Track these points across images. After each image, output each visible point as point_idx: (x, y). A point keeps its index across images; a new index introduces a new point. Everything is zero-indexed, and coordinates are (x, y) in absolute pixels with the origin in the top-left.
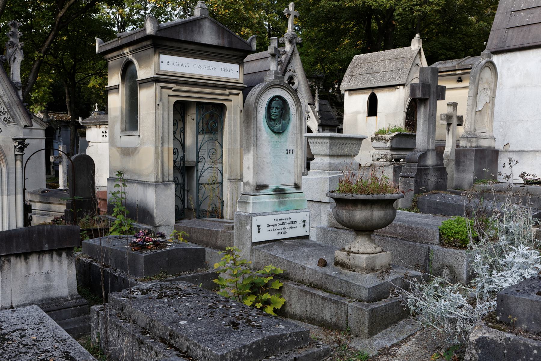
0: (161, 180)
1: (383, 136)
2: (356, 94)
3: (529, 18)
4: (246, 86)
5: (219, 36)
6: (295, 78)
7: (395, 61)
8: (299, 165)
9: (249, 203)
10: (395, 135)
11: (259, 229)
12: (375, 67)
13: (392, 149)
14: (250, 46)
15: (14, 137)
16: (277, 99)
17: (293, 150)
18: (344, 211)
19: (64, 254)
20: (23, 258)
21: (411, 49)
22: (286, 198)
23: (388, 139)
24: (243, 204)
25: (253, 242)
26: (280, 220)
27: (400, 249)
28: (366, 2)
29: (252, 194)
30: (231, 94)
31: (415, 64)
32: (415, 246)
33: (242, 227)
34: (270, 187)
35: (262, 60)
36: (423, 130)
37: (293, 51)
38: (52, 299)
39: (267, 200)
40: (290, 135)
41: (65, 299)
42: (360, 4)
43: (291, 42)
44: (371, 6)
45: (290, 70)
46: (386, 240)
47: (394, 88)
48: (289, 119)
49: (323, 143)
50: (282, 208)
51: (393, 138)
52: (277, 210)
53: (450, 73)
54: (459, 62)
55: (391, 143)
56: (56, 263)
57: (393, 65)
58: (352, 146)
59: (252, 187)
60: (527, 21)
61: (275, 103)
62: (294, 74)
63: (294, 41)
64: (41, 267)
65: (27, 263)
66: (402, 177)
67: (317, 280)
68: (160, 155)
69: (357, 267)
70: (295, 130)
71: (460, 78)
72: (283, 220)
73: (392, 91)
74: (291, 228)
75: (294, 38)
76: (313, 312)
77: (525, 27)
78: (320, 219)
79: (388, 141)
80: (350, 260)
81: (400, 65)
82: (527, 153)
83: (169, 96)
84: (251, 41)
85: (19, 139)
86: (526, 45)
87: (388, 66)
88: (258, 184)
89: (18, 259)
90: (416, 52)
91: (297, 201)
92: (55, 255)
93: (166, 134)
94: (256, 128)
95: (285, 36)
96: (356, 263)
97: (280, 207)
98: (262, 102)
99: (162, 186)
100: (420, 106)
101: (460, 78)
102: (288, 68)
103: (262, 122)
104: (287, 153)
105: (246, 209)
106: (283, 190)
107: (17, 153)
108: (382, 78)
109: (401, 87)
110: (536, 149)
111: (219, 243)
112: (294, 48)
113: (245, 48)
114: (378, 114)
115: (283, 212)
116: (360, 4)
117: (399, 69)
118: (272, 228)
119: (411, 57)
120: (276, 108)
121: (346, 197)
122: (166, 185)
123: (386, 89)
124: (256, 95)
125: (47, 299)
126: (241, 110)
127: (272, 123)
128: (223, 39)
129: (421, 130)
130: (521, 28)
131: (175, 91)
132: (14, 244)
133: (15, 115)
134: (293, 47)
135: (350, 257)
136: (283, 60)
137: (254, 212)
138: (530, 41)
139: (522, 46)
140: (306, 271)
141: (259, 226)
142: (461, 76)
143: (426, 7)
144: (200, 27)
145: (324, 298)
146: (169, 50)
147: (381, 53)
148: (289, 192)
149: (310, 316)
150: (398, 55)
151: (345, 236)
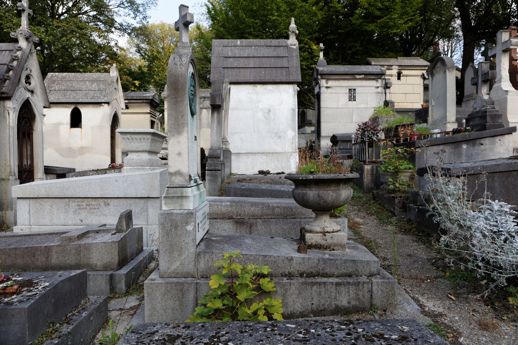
2: (57, 107)
3: (237, 63)
9: (186, 197)
12: (76, 85)
18: (330, 192)
21: (110, 75)
24: (175, 199)
27: (285, 227)
32: (301, 222)
33: (176, 228)
43: (27, 39)
45: (27, 68)
46: (269, 221)
47: (98, 106)
49: (142, 139)
57: (95, 86)
60: (235, 65)
62: (31, 73)
63: (31, 39)
66: (208, 170)
67: (312, 267)
69: (335, 245)
73: (97, 107)
76: (323, 302)
77: (236, 69)
78: (147, 215)
80: (326, 241)
81: (102, 86)
82: (242, 155)
86: (240, 81)
87: (90, 86)
96: (335, 242)
105: (181, 205)
108: (86, 95)
109: (106, 105)
110: (248, 152)
112: (32, 46)
114: (82, 126)
121: (339, 177)
123: (91, 106)
129: (215, 132)
130: (233, 69)
135: (327, 237)
138: (242, 79)
139: (237, 81)
140: (294, 261)
142: (127, 104)
145: (338, 284)
149: (318, 309)
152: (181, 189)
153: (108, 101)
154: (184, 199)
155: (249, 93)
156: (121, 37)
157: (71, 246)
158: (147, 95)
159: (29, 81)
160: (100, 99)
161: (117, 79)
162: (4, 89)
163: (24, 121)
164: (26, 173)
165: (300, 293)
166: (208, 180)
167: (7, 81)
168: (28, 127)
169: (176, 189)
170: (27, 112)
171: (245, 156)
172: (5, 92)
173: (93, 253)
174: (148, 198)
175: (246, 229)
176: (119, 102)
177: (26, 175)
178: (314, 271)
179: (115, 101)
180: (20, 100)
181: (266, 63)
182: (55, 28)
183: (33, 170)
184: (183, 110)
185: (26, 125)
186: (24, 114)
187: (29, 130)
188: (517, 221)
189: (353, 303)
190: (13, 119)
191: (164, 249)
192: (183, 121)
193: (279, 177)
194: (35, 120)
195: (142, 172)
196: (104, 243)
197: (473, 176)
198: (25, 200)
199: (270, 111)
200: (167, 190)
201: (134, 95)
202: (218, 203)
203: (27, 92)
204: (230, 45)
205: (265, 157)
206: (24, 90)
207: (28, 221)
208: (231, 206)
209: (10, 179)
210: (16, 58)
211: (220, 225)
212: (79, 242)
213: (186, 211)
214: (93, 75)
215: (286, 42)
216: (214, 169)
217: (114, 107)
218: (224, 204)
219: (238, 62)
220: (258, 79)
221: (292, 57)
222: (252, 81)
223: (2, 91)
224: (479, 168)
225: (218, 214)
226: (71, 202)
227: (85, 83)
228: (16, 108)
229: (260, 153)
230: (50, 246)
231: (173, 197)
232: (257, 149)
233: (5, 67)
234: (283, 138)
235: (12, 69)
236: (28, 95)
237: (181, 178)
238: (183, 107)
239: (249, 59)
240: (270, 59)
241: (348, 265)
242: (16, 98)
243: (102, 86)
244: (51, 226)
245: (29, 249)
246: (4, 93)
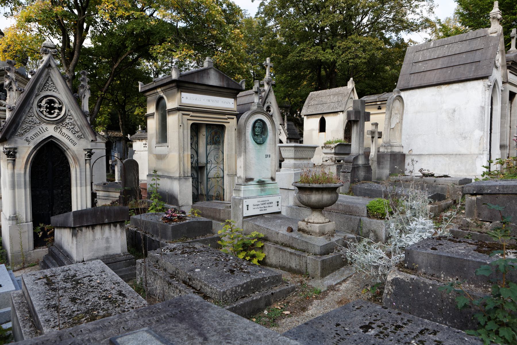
0: (182, 176)
1: (330, 145)
3: (425, 67)
5: (220, 80)
6: (271, 107)
9: (241, 190)
12: (324, 100)
13: (335, 154)
14: (241, 86)
15: (84, 148)
16: (259, 121)
19: (118, 226)
20: (90, 228)
27: (341, 220)
30: (229, 118)
32: (351, 218)
33: (236, 206)
34: (255, 180)
36: (356, 142)
38: (111, 256)
41: (119, 255)
43: (268, 84)
44: (321, 60)
47: (336, 114)
50: (263, 193)
51: (336, 147)
53: (373, 103)
55: (335, 150)
56: (113, 231)
57: (335, 99)
60: (423, 69)
63: (270, 83)
64: (103, 234)
65: (93, 231)
66: (342, 172)
68: (182, 159)
69: (313, 232)
74: (269, 206)
77: (422, 73)
78: (288, 201)
79: (333, 148)
81: (340, 98)
83: (188, 120)
84: (242, 83)
85: (88, 149)
88: (247, 178)
89: (88, 229)
90: (351, 90)
91: (273, 189)
92: (112, 226)
93: (186, 145)
94: (245, 140)
95: (264, 80)
96: (312, 229)
97: (261, 193)
99: (183, 180)
100: (353, 125)
101: (379, 107)
105: (239, 195)
106: (263, 181)
107: (86, 158)
109: (341, 113)
110: (430, 153)
113: (238, 88)
119: (348, 93)
120: (259, 127)
121: (305, 186)
122: (186, 179)
123: (332, 115)
125: (107, 256)
127: (256, 137)
128: (223, 82)
131: (191, 116)
132: (85, 219)
133: (85, 133)
134: (270, 86)
138: (426, 82)
141: (248, 206)
144: (208, 74)
145: (291, 253)
146: (188, 89)
153: (342, 110)
155: (433, 95)
161: (353, 90)
165: (274, 253)
171: (426, 157)
174: (288, 189)
178: (287, 243)
181: (456, 61)
188: (516, 251)
189: (298, 267)
193: (434, 181)
195: (289, 172)
197: (491, 196)
199: (454, 111)
204: (423, 49)
205: (448, 159)
215: (486, 31)
219: (426, 65)
220: (441, 80)
221: (489, 47)
222: (434, 83)
224: (497, 188)
227: (330, 97)
229: (442, 154)
232: (439, 150)
234: (468, 138)
239: (438, 59)
240: (461, 55)
241: (304, 244)
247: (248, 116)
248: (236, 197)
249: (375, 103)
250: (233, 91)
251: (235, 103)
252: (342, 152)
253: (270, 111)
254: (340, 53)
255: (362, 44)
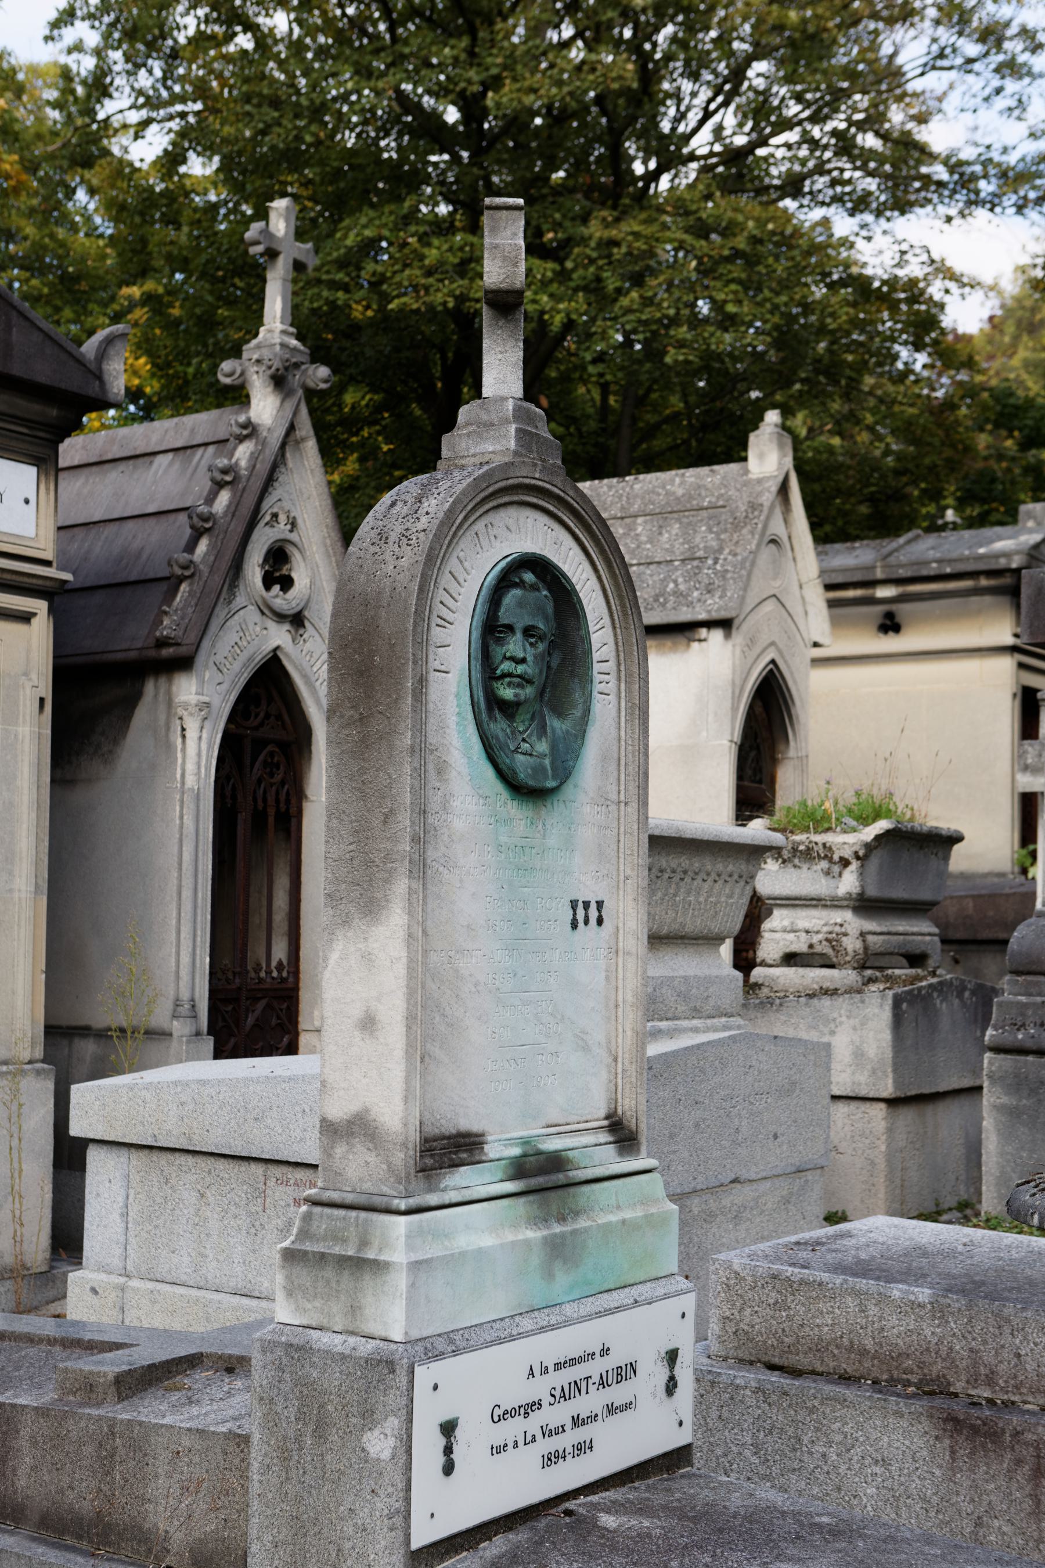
4: (67, 576)
6: (296, 557)
7: (679, 520)
8: (630, 998)
9: (378, 1267)
10: (878, 838)
11: (448, 1450)
14: (98, 376)
16: (529, 577)
17: (600, 904)
21: (747, 472)
22: (577, 1213)
23: (847, 853)
24: (329, 1273)
25: (415, 1545)
26: (558, 1366)
28: (470, 300)
29: (403, 1205)
31: (767, 539)
33: (320, 1433)
34: (492, 1150)
35: (122, 466)
37: (291, 428)
39: (487, 1241)
40: (587, 809)
42: (445, 303)
43: (279, 381)
45: (275, 516)
47: (681, 640)
48: (587, 711)
50: (563, 1279)
52: (538, 1303)
53: (851, 593)
54: (885, 551)
55: (862, 874)
58: (717, 886)
59: (399, 1158)
61: (520, 604)
62: (293, 537)
63: (296, 379)
66: (997, 1049)
70: (613, 779)
71: (890, 615)
72: (573, 1362)
73: (674, 649)
74: (611, 1410)
75: (297, 366)
79: (845, 863)
81: (704, 537)
84: (103, 353)
87: (650, 541)
88: (431, 1131)
90: (774, 487)
94: (421, 750)
95: (249, 349)
97: (549, 1275)
98: (453, 587)
101: (890, 615)
102: (265, 505)
103: (452, 720)
104: (574, 925)
105: (354, 1310)
106: (556, 1162)
109: (716, 636)
111: (21, 1483)
112: (296, 413)
113: (72, 382)
115: (569, 1310)
116: (445, 303)
117: (700, 554)
118: (514, 1428)
119: (754, 506)
124: (425, 540)
126: (42, 700)
127: (499, 727)
134: (290, 406)
136: (243, 463)
137: (415, 1334)
141: (448, 1429)
142: (894, 607)
143: (712, 335)
147: (610, 487)
148: (599, 1172)
150: (691, 498)
151: (859, 1426)
152: (363, 1215)
153: (723, 614)
154: (367, 1277)
156: (956, 222)
157: (83, 1424)
158: (1000, 545)
159: (284, 572)
160: (690, 604)
161: (784, 490)
162: (168, 627)
163: (261, 758)
164: (261, 1005)
166: (996, 1107)
167: (184, 587)
168: (283, 783)
169: (341, 1212)
170: (279, 717)
172: (168, 637)
173: (156, 1476)
175: (1010, 1477)
176: (797, 610)
177: (258, 1013)
179: (770, 606)
180: (237, 666)
182: (594, 255)
183: (296, 989)
184: (389, 786)
185: (272, 775)
186: (262, 724)
187: (283, 797)
190: (199, 755)
191: (267, 1538)
192: (388, 845)
194: (310, 752)
196: (201, 1432)
198: (115, 1152)
200: (307, 1218)
201: (932, 554)
202: (862, 1283)
203: (271, 625)
206: (256, 616)
207: (118, 1251)
208: (939, 1311)
209: (175, 1034)
210: (228, 478)
211: (859, 1426)
212: (123, 1413)
213: (372, 1344)
214: (672, 481)
216: (1030, 1044)
217: (764, 639)
218: (897, 1291)
223: (158, 634)
225: (864, 1352)
226: (271, 1183)
228: (216, 701)
230: (13, 1406)
231: (323, 1256)
233: (182, 525)
235: (207, 530)
236: (279, 636)
237: (371, 1158)
238: (391, 771)
242: (219, 658)
243: (704, 537)
244: (194, 1292)
245: (457, 1337)
246: (162, 643)
247: (450, 513)
248: (324, 1340)
249: (858, 593)
250: (33, 409)
251: (47, 500)
252: (899, 892)
253: (287, 583)
254: (612, 283)
255: (741, 242)
